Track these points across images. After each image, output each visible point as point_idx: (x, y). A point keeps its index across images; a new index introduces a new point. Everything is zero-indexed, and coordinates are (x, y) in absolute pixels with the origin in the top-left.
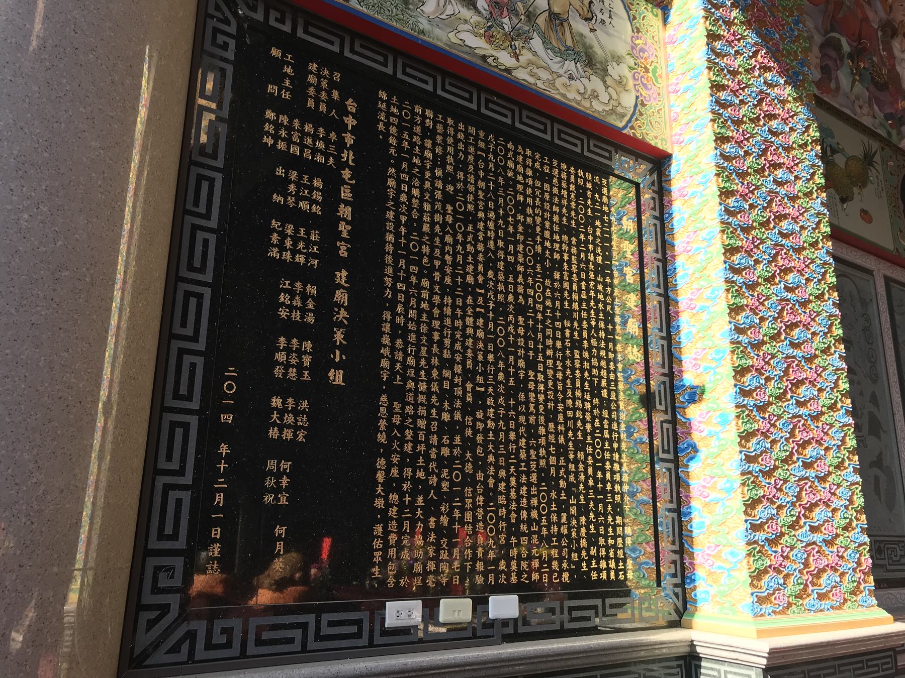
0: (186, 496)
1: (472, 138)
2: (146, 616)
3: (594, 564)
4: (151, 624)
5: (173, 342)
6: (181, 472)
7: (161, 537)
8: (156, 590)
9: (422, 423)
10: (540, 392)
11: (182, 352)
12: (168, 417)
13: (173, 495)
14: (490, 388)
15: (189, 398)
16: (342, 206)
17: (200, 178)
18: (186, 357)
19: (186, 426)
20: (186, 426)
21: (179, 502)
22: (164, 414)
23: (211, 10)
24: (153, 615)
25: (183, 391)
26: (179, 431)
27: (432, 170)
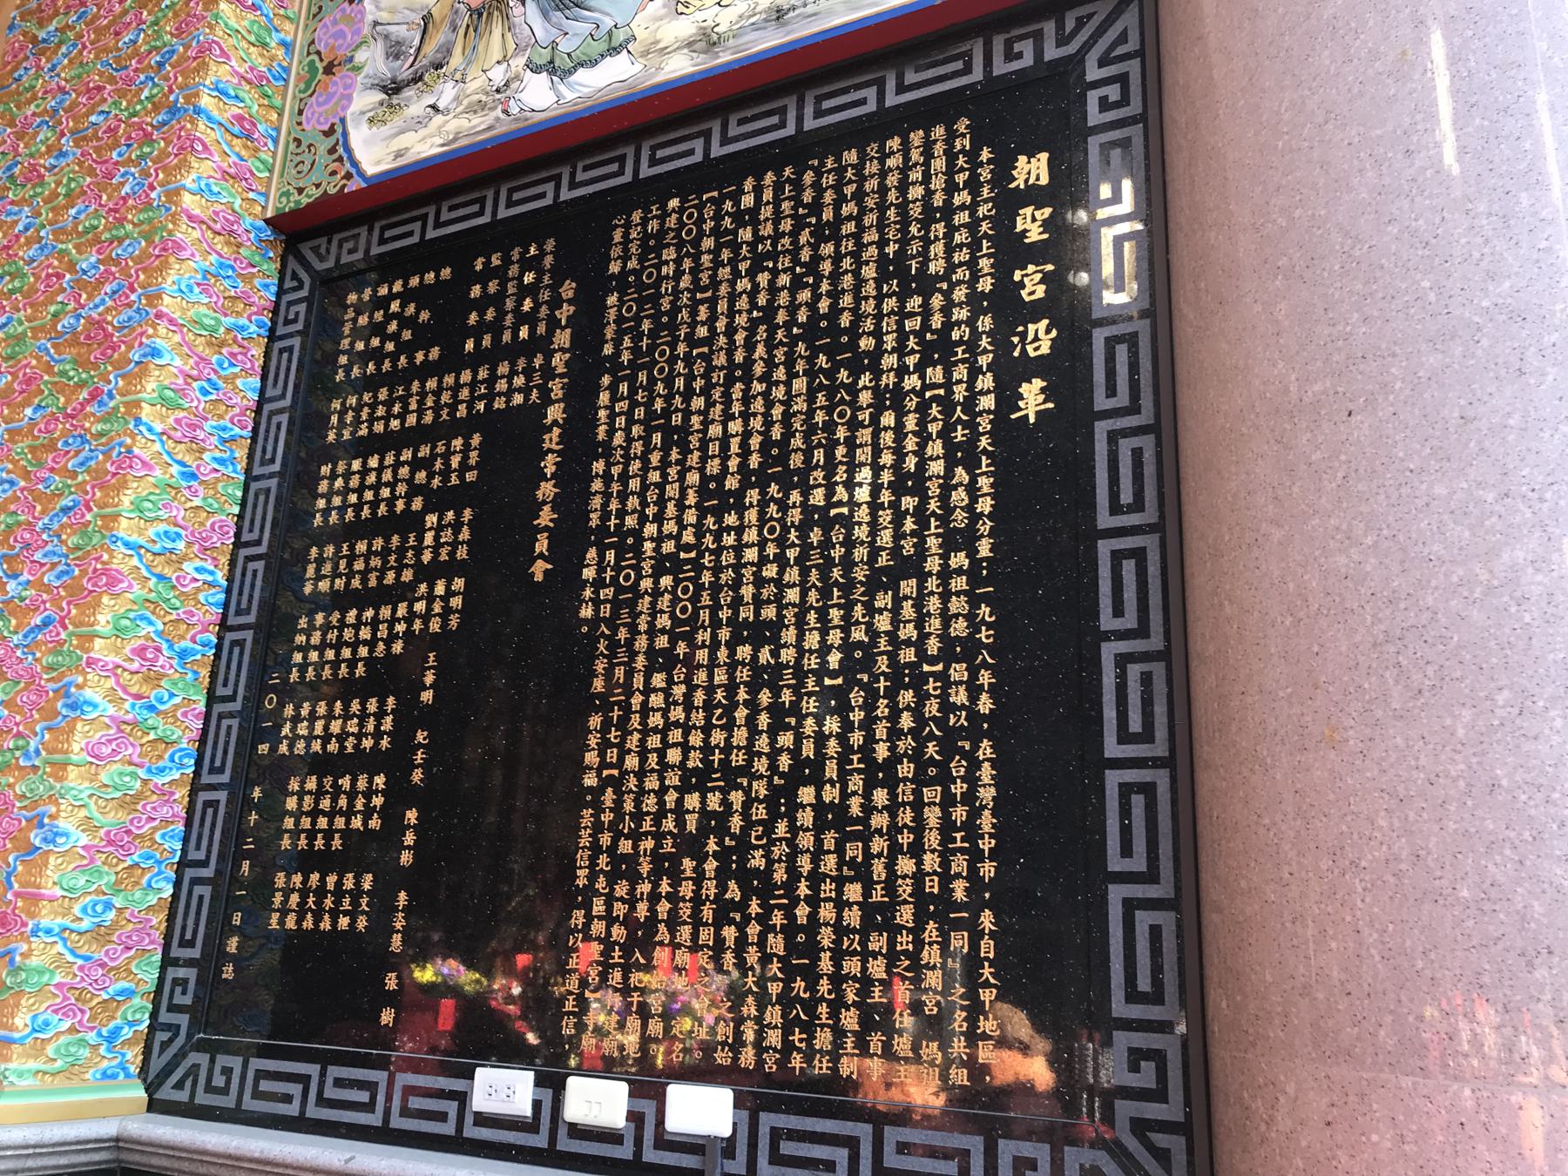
0: (1107, 622)
1: (855, 758)
2: (1132, 45)
3: (432, 659)
4: (1123, 38)
5: (1180, 1117)
6: (1122, 661)
7: (1139, 555)
8: (1123, 79)
9: (793, 595)
10: (600, 918)
11: (1142, 631)
12: (1159, 749)
13: (1130, 621)
14: (719, 691)
15: (1126, 790)
16: (993, 408)
17: (1138, 505)
18: (1143, 868)
19: (1124, 737)
20: (1124, 737)
21: (1118, 612)
22: (1167, 754)
23: (1174, 1143)
24: (1119, 51)
25: (1138, 801)
26: (1135, 725)
27: (892, 694)
